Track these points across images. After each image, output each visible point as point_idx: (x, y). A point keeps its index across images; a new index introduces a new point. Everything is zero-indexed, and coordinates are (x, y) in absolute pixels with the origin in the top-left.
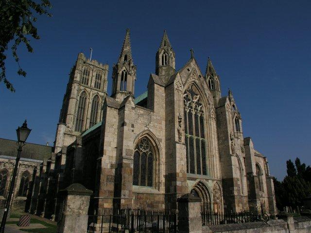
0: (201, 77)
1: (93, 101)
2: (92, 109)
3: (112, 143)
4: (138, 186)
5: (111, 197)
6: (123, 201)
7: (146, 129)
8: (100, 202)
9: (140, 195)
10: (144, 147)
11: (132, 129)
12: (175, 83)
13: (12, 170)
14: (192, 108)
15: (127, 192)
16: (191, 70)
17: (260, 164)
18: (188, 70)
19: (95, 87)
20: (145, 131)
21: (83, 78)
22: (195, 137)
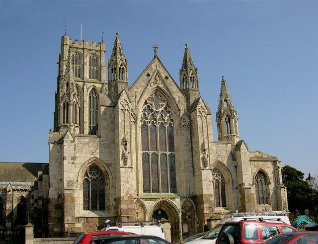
0: (168, 78)
1: (90, 97)
2: (90, 107)
3: (57, 176)
4: (89, 211)
5: (285, 212)
6: (66, 226)
7: (92, 156)
8: (50, 227)
9: (88, 219)
10: (94, 173)
11: (72, 161)
12: (119, 103)
13: (19, 193)
14: (155, 119)
15: (70, 218)
16: (151, 74)
17: (266, 170)
18: (148, 75)
19: (90, 78)
20: (91, 159)
21: (80, 64)
22: (160, 153)
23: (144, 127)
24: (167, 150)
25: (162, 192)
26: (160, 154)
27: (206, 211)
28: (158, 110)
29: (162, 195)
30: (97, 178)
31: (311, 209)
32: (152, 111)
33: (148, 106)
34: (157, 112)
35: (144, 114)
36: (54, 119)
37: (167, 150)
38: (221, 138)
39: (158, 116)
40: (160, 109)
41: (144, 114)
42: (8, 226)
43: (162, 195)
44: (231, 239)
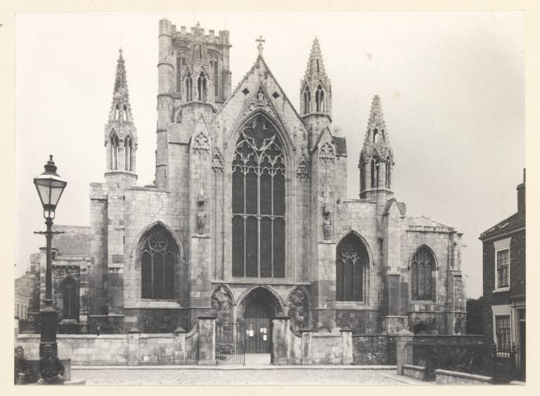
14: (256, 164)
23: (237, 177)
24: (272, 213)
25: (275, 276)
26: (245, 217)
27: (53, 280)
28: (261, 150)
29: (259, 280)
30: (162, 252)
31: (187, 280)
32: (251, 150)
33: (245, 143)
34: (259, 153)
35: (238, 156)
36: (519, 199)
37: (272, 213)
38: (363, 195)
39: (260, 159)
40: (263, 148)
41: (266, 158)
42: (83, 320)
43: (259, 280)
44: (265, 338)
